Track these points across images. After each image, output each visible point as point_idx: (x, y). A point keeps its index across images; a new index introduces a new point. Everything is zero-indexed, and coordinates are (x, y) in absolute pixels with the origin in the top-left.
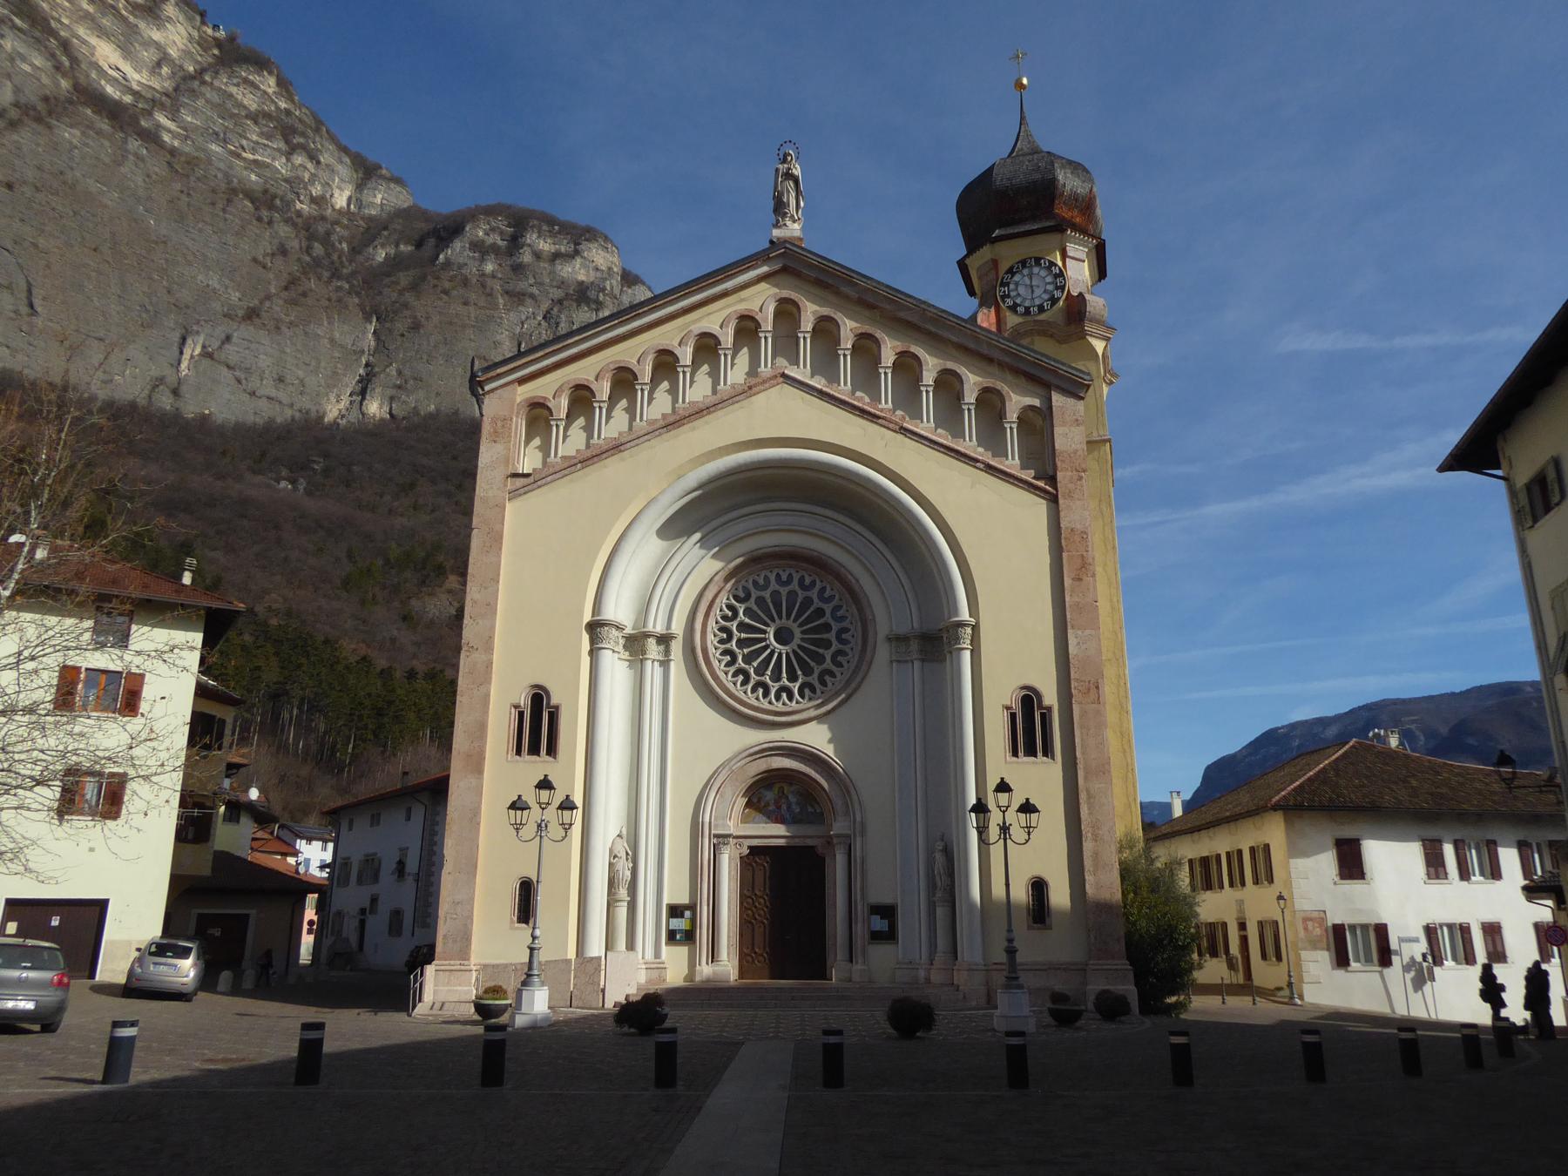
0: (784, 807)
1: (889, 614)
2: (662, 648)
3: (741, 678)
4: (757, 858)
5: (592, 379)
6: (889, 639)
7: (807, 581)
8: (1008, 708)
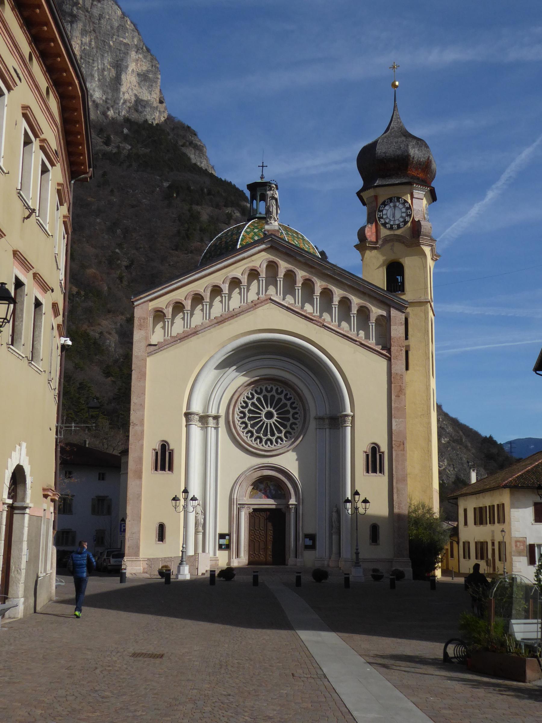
0: (268, 491)
1: (315, 407)
2: (215, 421)
3: (250, 434)
4: (256, 514)
5: (183, 299)
8: (365, 452)
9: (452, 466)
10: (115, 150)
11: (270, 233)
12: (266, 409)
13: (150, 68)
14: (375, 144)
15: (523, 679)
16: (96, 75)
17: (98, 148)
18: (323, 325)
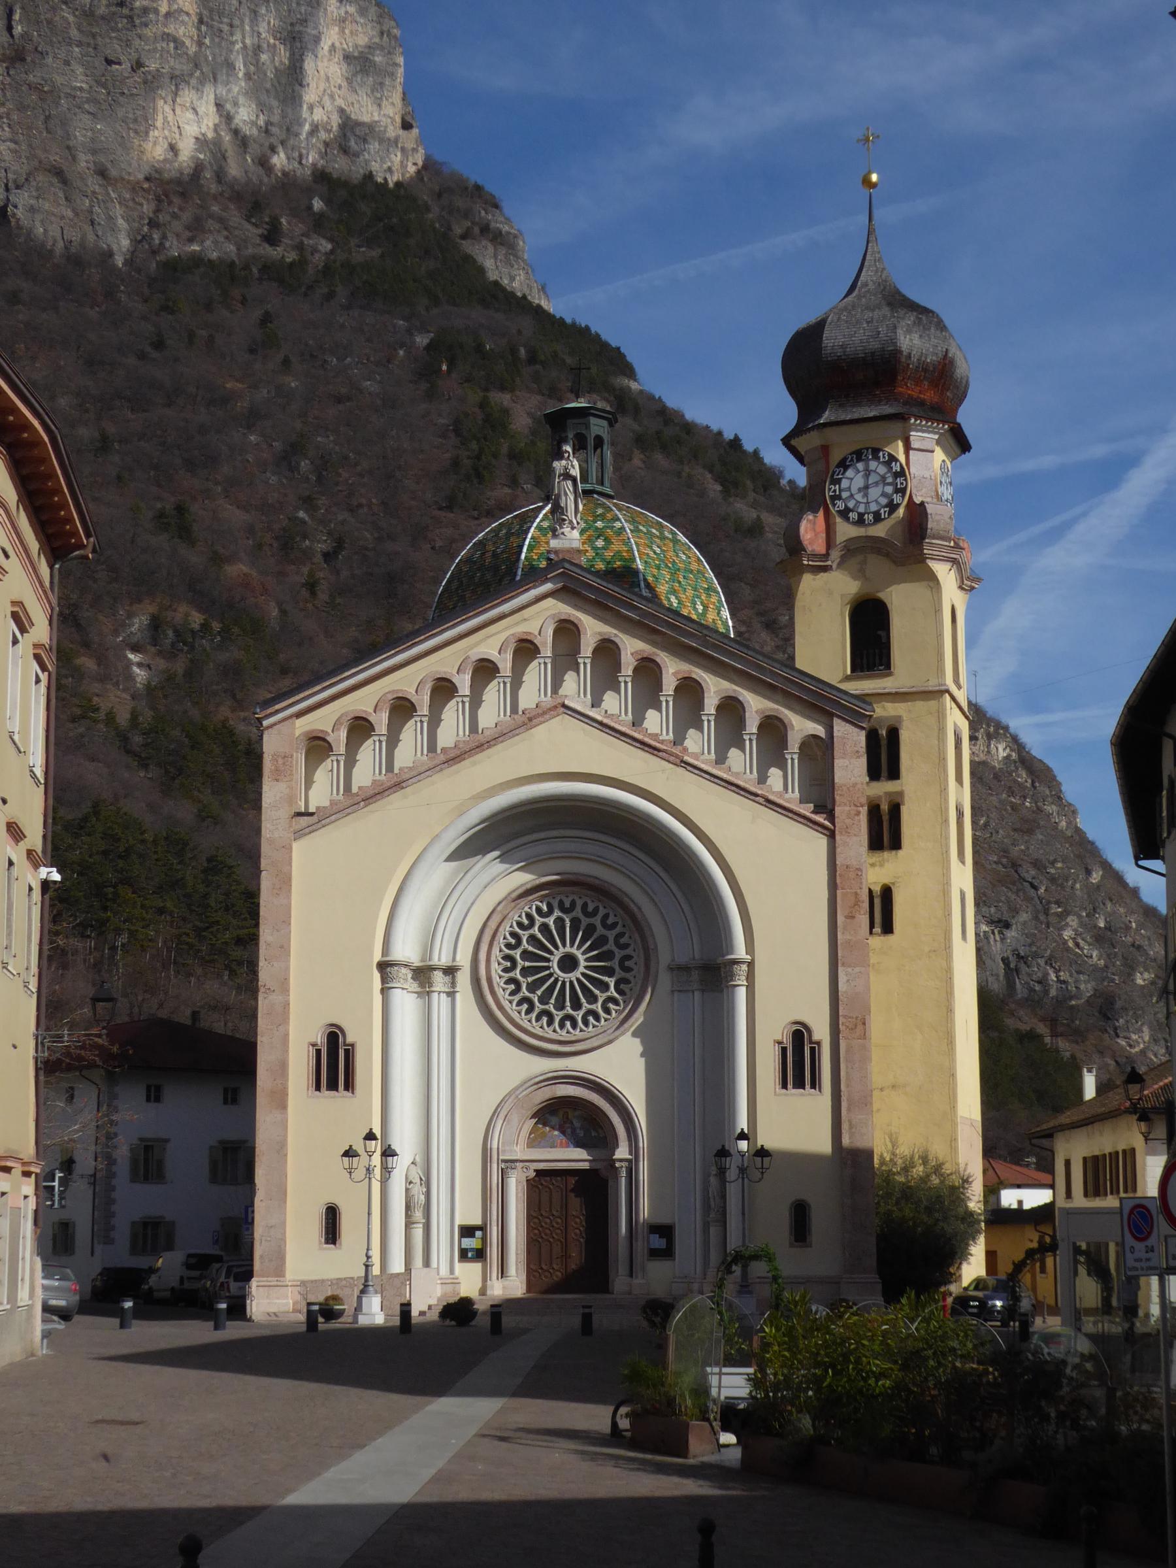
1: (670, 944)
2: (448, 979)
3: (525, 1006)
4: (544, 1183)
5: (371, 711)
6: (671, 969)
7: (590, 908)
8: (779, 1043)
9: (1162, 1042)
10: (291, 257)
11: (561, 557)
12: (561, 949)
13: (377, 40)
14: (820, 325)
15: (683, 1452)
16: (240, 64)
17: (250, 251)
18: (682, 761)
